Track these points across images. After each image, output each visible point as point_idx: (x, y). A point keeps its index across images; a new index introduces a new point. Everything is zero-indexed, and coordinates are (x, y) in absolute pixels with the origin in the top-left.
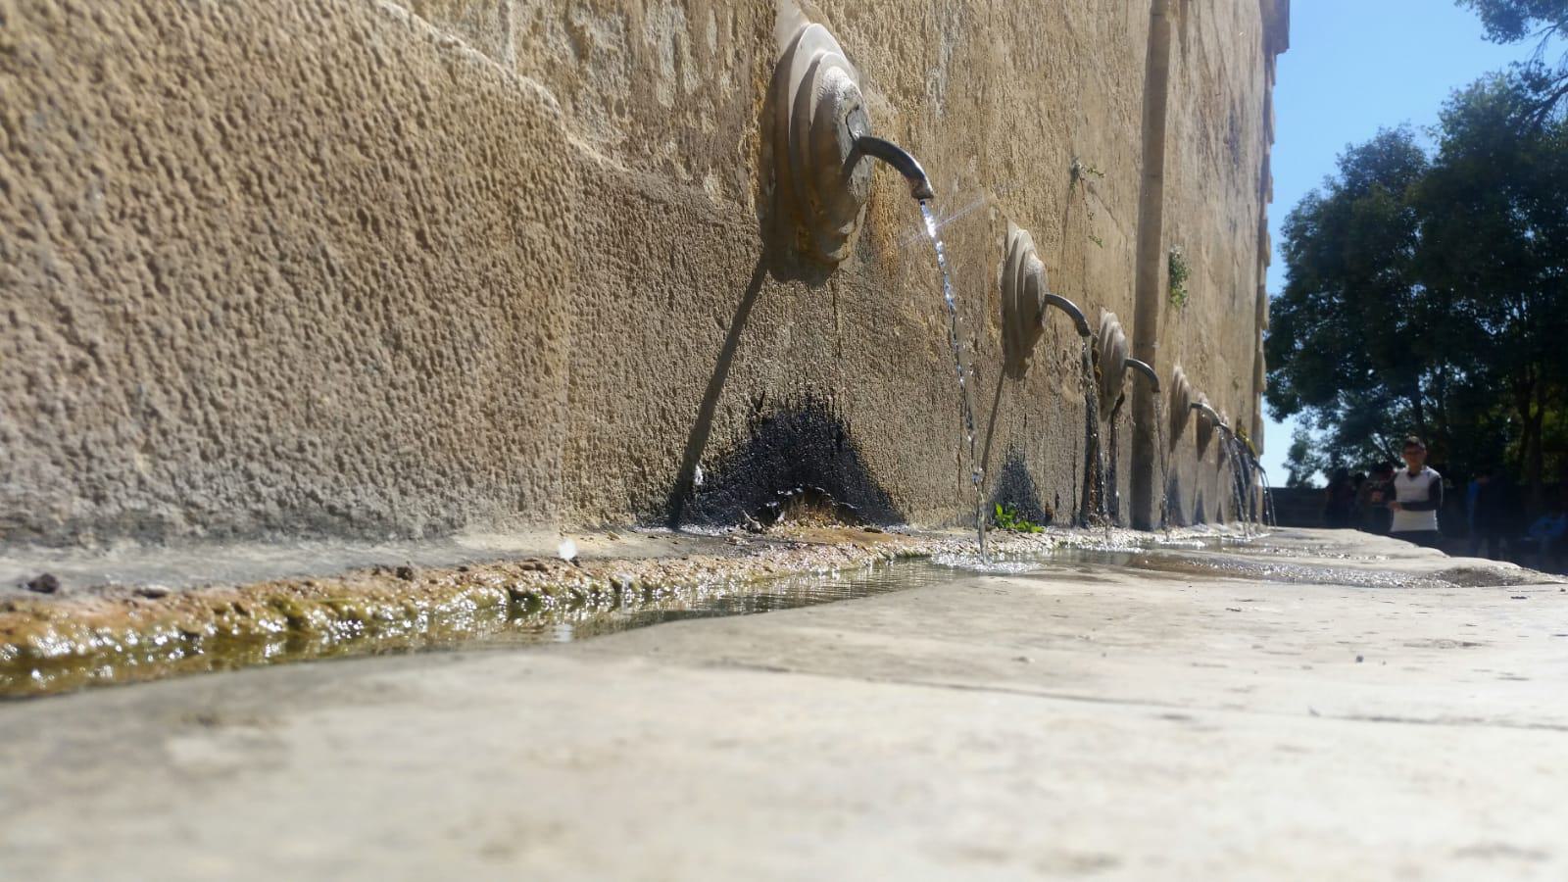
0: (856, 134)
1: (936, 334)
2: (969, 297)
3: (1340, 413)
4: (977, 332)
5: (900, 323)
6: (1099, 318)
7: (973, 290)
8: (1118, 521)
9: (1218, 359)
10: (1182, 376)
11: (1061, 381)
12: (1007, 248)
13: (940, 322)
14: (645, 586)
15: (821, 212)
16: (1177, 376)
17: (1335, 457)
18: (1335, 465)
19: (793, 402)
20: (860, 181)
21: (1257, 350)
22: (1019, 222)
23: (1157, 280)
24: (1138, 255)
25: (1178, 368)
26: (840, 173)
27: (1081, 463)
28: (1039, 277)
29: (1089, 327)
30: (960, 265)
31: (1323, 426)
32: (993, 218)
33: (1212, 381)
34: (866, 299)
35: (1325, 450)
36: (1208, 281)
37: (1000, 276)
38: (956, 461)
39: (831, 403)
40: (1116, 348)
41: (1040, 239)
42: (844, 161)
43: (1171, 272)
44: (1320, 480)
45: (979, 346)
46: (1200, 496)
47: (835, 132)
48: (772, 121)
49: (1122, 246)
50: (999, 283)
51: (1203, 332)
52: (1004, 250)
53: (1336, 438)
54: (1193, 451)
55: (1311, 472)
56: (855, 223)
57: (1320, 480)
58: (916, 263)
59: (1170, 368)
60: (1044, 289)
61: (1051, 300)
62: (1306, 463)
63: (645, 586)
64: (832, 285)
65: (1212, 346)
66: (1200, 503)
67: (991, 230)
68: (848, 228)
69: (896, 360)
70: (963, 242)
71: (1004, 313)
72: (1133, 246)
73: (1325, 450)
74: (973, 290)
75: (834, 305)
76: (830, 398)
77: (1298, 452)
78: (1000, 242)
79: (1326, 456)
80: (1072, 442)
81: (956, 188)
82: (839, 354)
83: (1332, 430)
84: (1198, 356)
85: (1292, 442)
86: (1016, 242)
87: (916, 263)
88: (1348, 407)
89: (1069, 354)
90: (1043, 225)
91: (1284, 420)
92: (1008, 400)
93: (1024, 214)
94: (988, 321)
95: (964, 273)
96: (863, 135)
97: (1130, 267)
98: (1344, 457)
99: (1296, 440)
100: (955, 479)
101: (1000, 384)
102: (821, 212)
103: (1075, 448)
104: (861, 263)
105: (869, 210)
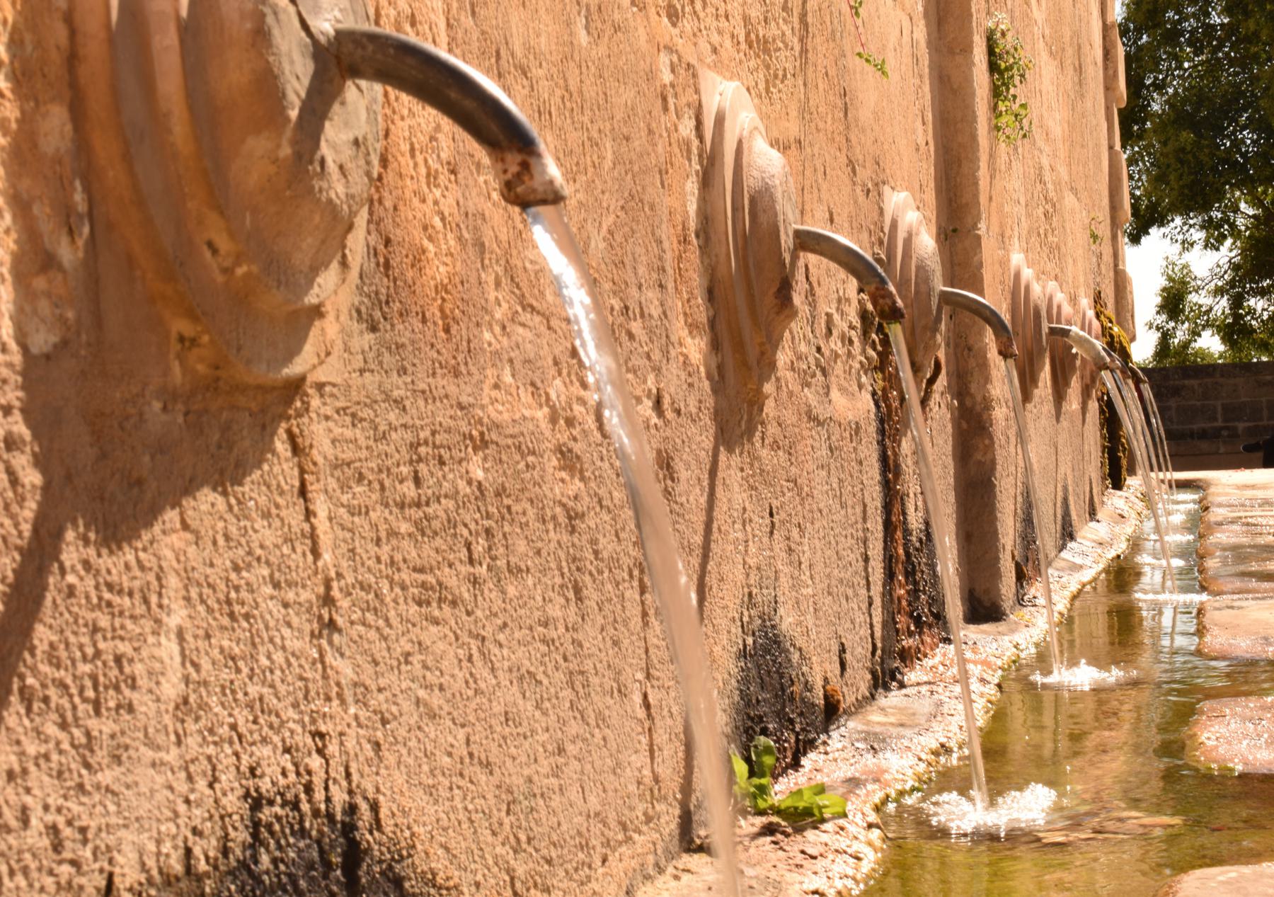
0: (325, 26)
1: (570, 422)
2: (633, 291)
3: (1240, 222)
4: (657, 370)
5: (482, 444)
6: (881, 212)
7: (642, 270)
8: (996, 752)
9: (1070, 200)
10: (1027, 273)
11: (827, 388)
12: (701, 137)
13: (576, 389)
14: (94, 625)
15: (241, 271)
16: (1017, 276)
17: (1237, 302)
18: (1237, 317)
19: (205, 848)
20: (348, 152)
21: (1111, 147)
22: (718, 67)
23: (973, 94)
24: (929, 43)
25: (1017, 258)
26: (286, 151)
27: (876, 525)
28: (779, 195)
29: (900, 303)
30: (609, 221)
31: (1213, 244)
32: (667, 77)
33: (1063, 249)
34: (392, 428)
35: (1219, 292)
36: (1044, 56)
37: (692, 208)
38: (641, 713)
39: (318, 781)
40: (921, 268)
41: (762, 86)
42: (294, 114)
43: (993, 67)
44: (1211, 344)
45: (666, 402)
46: (1065, 489)
47: (261, 36)
48: (60, 33)
49: (906, 38)
50: (692, 224)
51: (1045, 162)
52: (695, 143)
53: (1235, 267)
54: (1049, 407)
55: (1195, 333)
56: (344, 264)
57: (1211, 344)
58: (508, 268)
59: (1004, 263)
60: (790, 222)
61: (807, 241)
62: (1188, 319)
63: (94, 625)
64: (292, 437)
65: (1058, 184)
66: (1065, 500)
67: (666, 109)
68: (328, 279)
69: (480, 546)
70: (608, 164)
71: (711, 294)
72: (921, 34)
73: (1219, 292)
74: (642, 270)
75: (303, 492)
76: (316, 762)
77: (1173, 302)
78: (687, 128)
79: (1223, 304)
80: (859, 510)
81: (583, 38)
82: (332, 625)
83: (1227, 252)
84: (1041, 210)
85: (1163, 282)
86: (720, 120)
87: (508, 268)
88: (1251, 212)
89: (836, 317)
90: (767, 51)
91: (1144, 240)
92: (734, 495)
93: (728, 43)
94: (679, 329)
95: (618, 238)
96: (349, 24)
97: (921, 76)
98: (1252, 302)
99: (1170, 279)
100: (642, 759)
101: (713, 473)
102: (241, 271)
103: (865, 519)
104: (369, 337)
105: (374, 222)
